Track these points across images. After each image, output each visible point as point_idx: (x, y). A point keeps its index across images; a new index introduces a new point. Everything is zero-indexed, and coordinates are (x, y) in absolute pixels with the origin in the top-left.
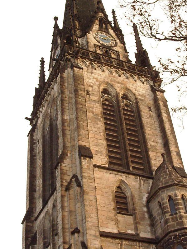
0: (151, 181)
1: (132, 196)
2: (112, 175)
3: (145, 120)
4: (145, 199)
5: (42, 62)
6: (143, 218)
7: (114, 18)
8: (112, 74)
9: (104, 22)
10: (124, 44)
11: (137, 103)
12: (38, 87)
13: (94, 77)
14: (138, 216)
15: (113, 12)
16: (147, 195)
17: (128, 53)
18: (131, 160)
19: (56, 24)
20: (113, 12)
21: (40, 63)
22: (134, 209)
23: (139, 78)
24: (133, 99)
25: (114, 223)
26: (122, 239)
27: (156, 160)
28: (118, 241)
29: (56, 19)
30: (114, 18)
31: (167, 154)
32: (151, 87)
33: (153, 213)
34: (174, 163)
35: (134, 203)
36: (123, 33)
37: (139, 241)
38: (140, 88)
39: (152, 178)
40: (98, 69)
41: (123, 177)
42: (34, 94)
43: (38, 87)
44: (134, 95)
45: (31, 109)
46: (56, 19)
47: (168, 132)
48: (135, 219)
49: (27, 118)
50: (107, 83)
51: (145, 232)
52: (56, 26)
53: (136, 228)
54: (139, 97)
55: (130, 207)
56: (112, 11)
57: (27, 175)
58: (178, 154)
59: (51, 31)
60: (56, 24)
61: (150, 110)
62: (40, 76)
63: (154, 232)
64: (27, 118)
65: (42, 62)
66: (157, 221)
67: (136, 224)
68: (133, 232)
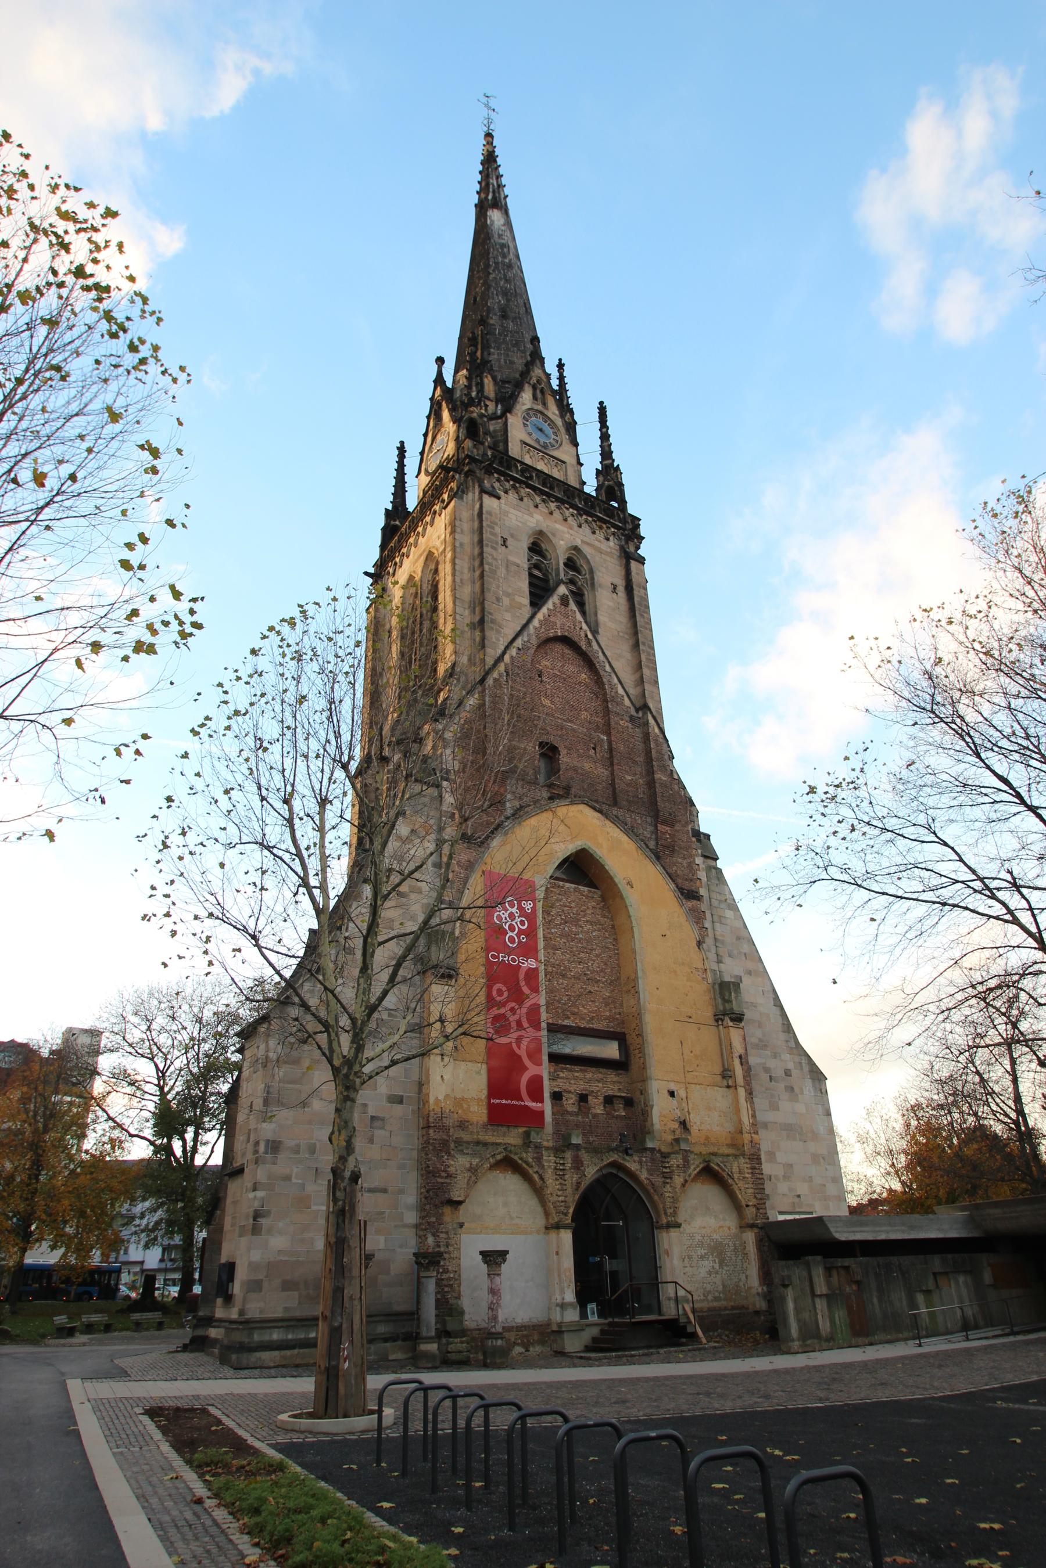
5: (402, 450)
7: (561, 378)
8: (566, 520)
9: (541, 389)
10: (576, 445)
12: (390, 507)
13: (517, 516)
15: (560, 366)
17: (582, 465)
18: (330, 932)
19: (440, 374)
20: (560, 366)
21: (397, 452)
29: (440, 361)
30: (561, 378)
34: (630, 908)
38: (599, 549)
43: (390, 507)
45: (375, 555)
46: (440, 361)
49: (366, 574)
52: (439, 380)
56: (557, 362)
57: (649, 623)
59: (428, 388)
60: (440, 374)
64: (366, 574)
65: (402, 450)
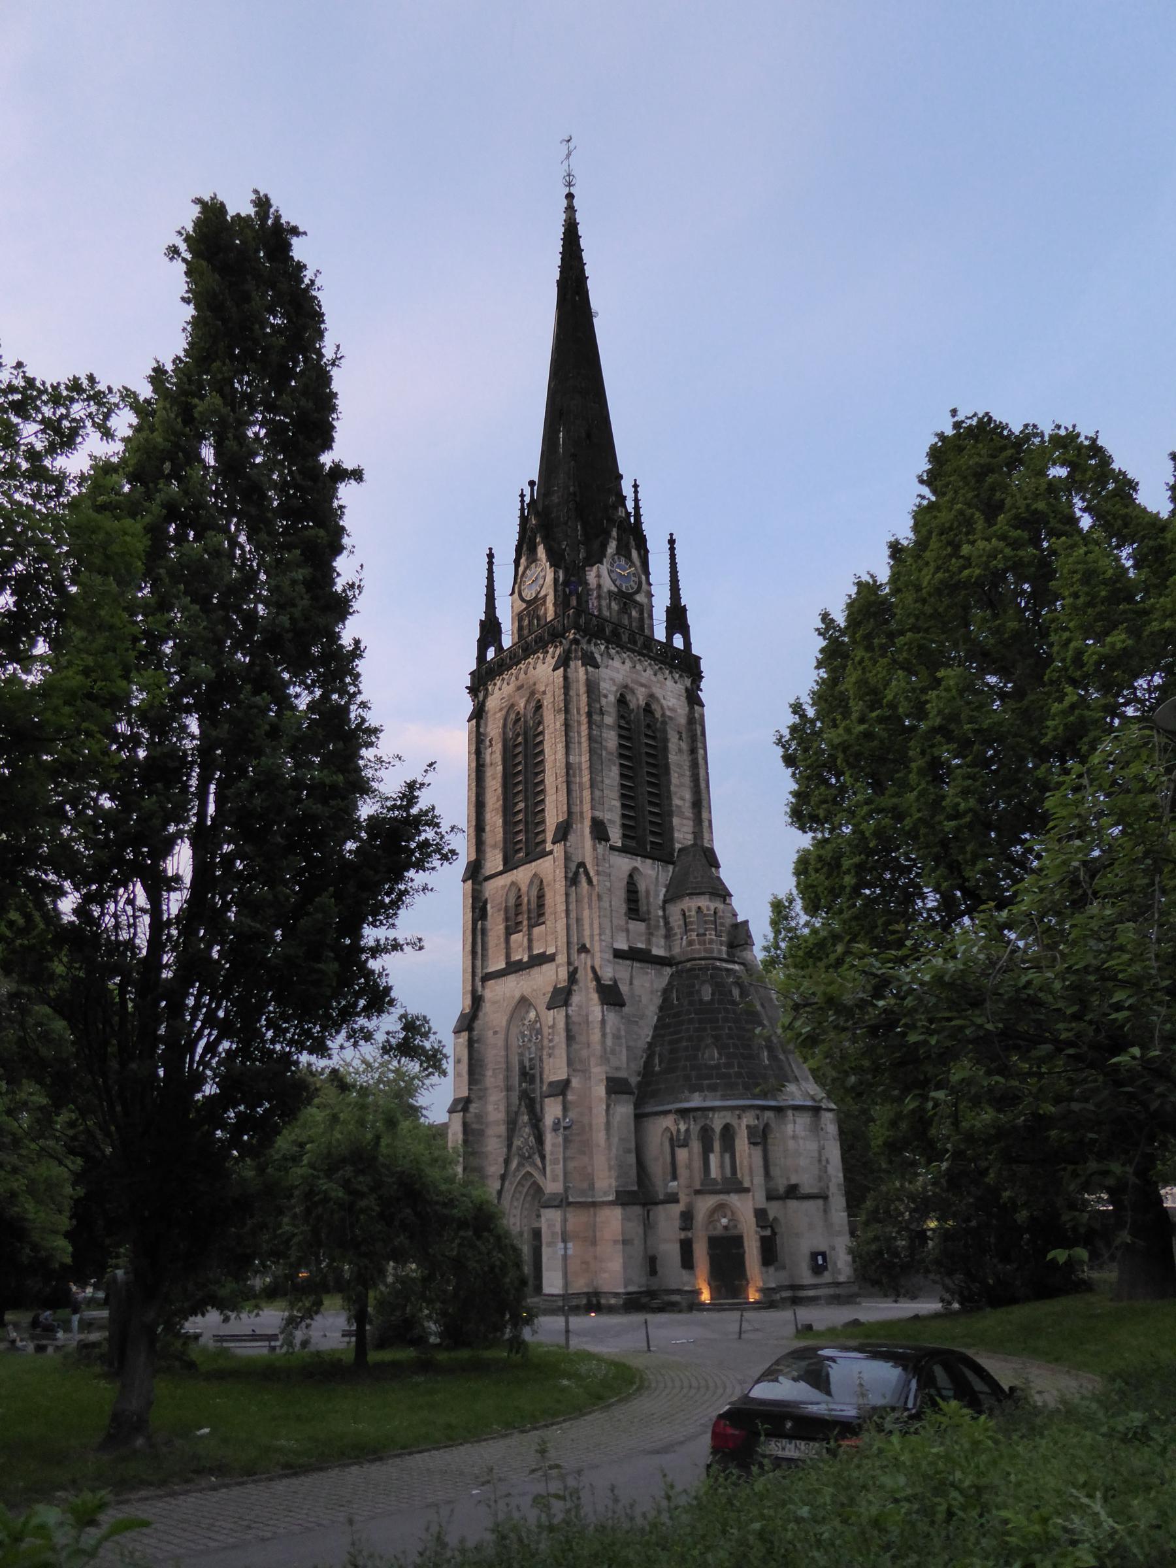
0: (671, 868)
1: (648, 892)
2: (626, 860)
3: (673, 758)
4: (661, 897)
6: (658, 927)
11: (664, 723)
14: (652, 923)
15: (636, 486)
16: (664, 890)
20: (636, 486)
22: (648, 912)
23: (671, 672)
24: (658, 715)
25: (624, 934)
26: (633, 959)
27: (682, 834)
28: (628, 962)
31: (698, 834)
32: (687, 690)
33: (671, 920)
35: (648, 904)
36: (649, 545)
37: (652, 963)
38: (669, 693)
39: (673, 863)
40: (616, 657)
41: (638, 862)
42: (478, 636)
44: (662, 708)
47: (703, 785)
48: (648, 927)
50: (626, 687)
51: (658, 946)
53: (649, 942)
54: (668, 713)
55: (643, 908)
58: (710, 822)
61: (680, 738)
62: (289, 246)
63: (669, 948)
66: (675, 934)
67: (650, 934)
68: (643, 946)
